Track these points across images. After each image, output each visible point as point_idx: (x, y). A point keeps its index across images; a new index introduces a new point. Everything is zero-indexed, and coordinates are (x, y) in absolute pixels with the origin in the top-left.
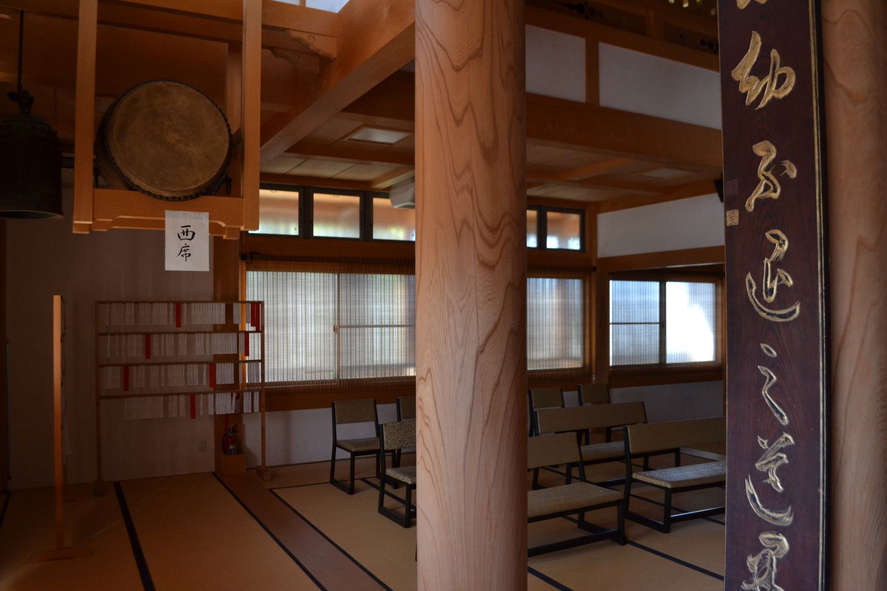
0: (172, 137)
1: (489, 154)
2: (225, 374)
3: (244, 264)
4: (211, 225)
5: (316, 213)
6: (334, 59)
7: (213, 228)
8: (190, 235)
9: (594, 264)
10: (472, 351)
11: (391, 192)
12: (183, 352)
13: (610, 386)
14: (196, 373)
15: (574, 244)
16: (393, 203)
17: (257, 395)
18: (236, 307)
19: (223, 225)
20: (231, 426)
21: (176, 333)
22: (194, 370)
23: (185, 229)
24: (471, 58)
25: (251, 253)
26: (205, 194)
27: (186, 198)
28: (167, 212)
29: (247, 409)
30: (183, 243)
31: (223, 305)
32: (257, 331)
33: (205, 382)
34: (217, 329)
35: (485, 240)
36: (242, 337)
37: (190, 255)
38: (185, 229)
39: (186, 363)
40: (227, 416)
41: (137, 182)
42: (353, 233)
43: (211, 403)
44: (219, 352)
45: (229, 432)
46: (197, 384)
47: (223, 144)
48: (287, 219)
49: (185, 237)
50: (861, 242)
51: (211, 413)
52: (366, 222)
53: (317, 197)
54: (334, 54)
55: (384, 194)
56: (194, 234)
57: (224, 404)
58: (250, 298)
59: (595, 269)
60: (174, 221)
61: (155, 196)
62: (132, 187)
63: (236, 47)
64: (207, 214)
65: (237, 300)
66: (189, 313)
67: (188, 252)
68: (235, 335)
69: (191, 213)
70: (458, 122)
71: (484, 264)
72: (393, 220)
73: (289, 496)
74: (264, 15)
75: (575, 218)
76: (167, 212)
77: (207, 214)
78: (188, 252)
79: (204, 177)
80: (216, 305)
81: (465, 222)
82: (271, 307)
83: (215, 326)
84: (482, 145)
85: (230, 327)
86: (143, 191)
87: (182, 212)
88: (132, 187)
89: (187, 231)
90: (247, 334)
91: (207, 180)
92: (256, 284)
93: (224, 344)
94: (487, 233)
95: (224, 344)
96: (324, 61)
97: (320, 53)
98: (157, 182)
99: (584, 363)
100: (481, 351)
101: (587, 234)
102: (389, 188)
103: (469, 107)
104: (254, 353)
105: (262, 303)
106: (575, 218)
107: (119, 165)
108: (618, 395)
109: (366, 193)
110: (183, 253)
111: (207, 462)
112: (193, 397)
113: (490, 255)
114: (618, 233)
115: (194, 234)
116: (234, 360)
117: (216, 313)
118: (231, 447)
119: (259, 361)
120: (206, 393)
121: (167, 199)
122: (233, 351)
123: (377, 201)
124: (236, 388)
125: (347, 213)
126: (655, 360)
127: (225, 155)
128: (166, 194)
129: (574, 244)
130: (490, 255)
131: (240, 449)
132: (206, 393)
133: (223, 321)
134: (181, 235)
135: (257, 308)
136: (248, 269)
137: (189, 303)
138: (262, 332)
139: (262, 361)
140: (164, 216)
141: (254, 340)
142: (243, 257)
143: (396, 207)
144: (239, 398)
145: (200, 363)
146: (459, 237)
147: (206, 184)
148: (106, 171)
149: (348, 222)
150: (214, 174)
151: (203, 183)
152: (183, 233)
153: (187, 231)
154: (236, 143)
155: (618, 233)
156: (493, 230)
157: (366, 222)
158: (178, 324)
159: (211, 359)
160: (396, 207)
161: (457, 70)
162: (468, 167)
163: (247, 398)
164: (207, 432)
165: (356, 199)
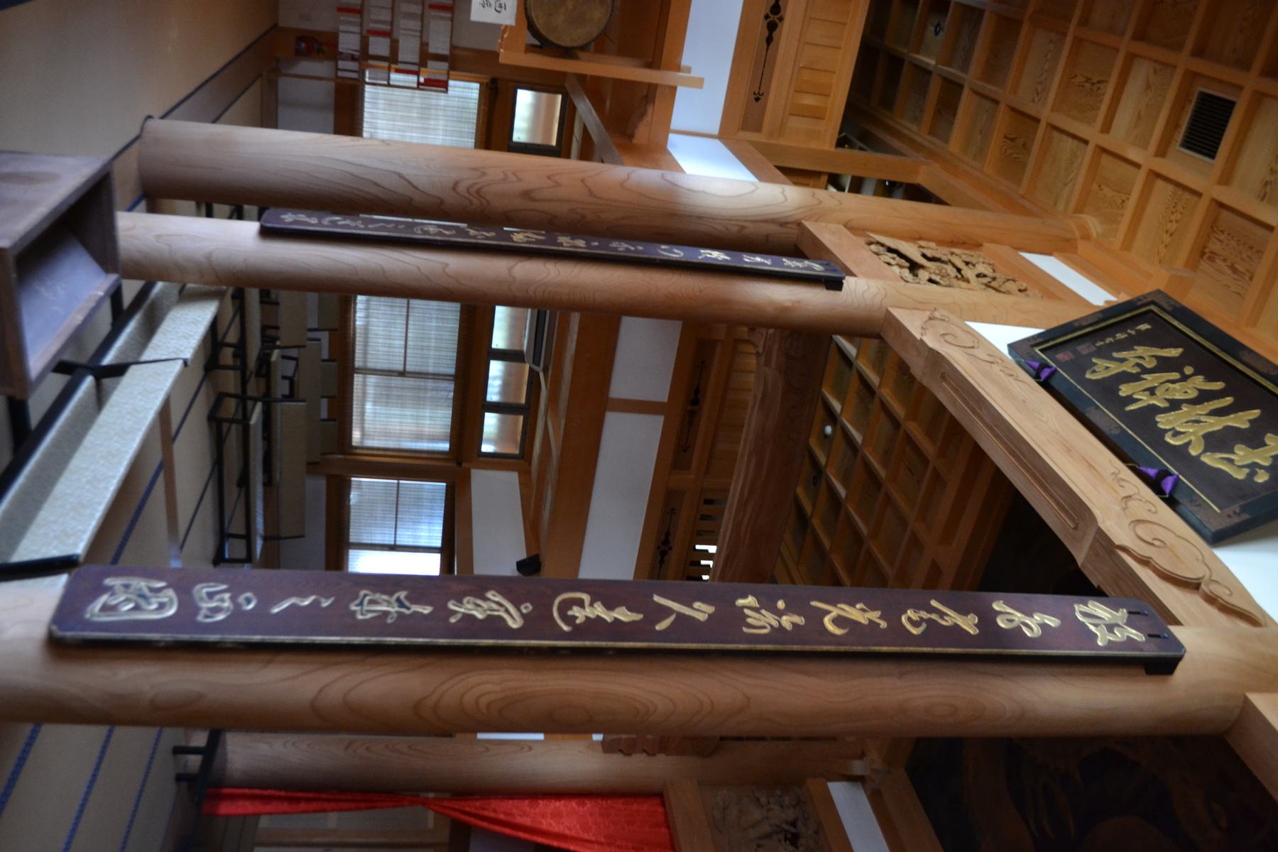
1: (527, 194)
2: (379, 46)
9: (464, 465)
10: (403, 171)
12: (404, 7)
13: (330, 478)
14: (382, 18)
15: (487, 448)
17: (355, 75)
18: (444, 66)
20: (325, 48)
21: (423, 4)
22: (385, 16)
24: (590, 191)
27: (526, 9)
29: (341, 64)
31: (447, 52)
32: (419, 83)
33: (373, 26)
34: (424, 45)
35: (471, 186)
36: (415, 68)
39: (393, 9)
40: (336, 46)
43: (351, 28)
44: (402, 44)
45: (319, 45)
46: (372, 17)
47: (566, 42)
50: (447, 265)
51: (342, 28)
54: (634, 141)
57: (349, 42)
58: (451, 83)
59: (459, 464)
63: (650, 65)
65: (452, 68)
66: (442, 18)
68: (416, 60)
69: (515, 11)
70: (549, 177)
71: (456, 184)
73: (255, 89)
75: (515, 451)
80: (447, 46)
81: (484, 174)
82: (442, 103)
83: (427, 44)
84: (533, 190)
85: (425, 57)
90: (417, 73)
92: (466, 93)
93: (408, 50)
94: (476, 187)
95: (408, 50)
96: (631, 136)
99: (356, 448)
100: (400, 176)
101: (496, 461)
103: (558, 185)
104: (396, 78)
105: (446, 92)
106: (515, 451)
108: (317, 487)
111: (290, 20)
112: (359, 11)
113: (462, 188)
114: (496, 496)
116: (392, 60)
117: (439, 45)
118: (303, 45)
119: (389, 80)
120: (361, 25)
122: (401, 57)
124: (364, 57)
126: (353, 539)
129: (487, 448)
130: (462, 188)
131: (300, 54)
132: (361, 25)
133: (432, 50)
135: (442, 85)
136: (481, 85)
137: (452, 20)
138: (418, 88)
139: (389, 85)
141: (411, 80)
142: (494, 81)
144: (353, 58)
145: (392, 23)
146: (475, 169)
155: (496, 496)
156: (478, 192)
158: (432, 7)
159: (395, 35)
161: (582, 181)
162: (520, 180)
163: (353, 65)
164: (320, 23)
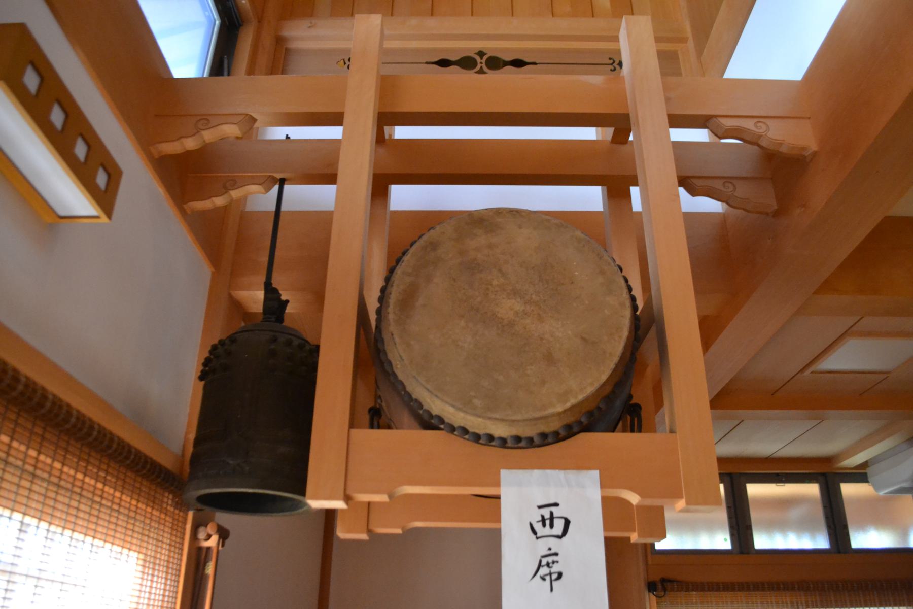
0: (508, 307)
3: (654, 598)
4: (605, 500)
5: (754, 515)
6: (815, 154)
7: (613, 509)
8: (559, 525)
11: (869, 471)
16: (877, 488)
19: (634, 499)
23: (546, 512)
25: (664, 580)
26: (588, 428)
27: (546, 439)
28: (504, 473)
30: (542, 547)
37: (560, 575)
38: (546, 512)
41: (436, 406)
42: (821, 542)
48: (710, 527)
49: (547, 531)
52: (836, 521)
53: (754, 490)
55: (859, 475)
56: (567, 523)
60: (522, 491)
61: (477, 438)
62: (429, 422)
64: (596, 474)
67: (556, 568)
72: (878, 516)
74: (668, 100)
76: (504, 473)
77: (596, 474)
78: (556, 568)
79: (586, 383)
86: (452, 429)
87: (537, 473)
88: (429, 422)
89: (552, 518)
91: (590, 390)
97: (784, 149)
98: (477, 402)
102: (865, 465)
107: (401, 376)
109: (828, 475)
110: (544, 571)
115: (567, 523)
121: (503, 443)
123: (848, 490)
125: (795, 513)
127: (625, 333)
128: (500, 431)
134: (538, 527)
140: (498, 484)
143: (881, 493)
147: (587, 399)
148: (383, 402)
149: (803, 526)
150: (604, 378)
151: (581, 397)
152: (543, 520)
153: (552, 518)
154: (645, 326)
157: (836, 521)
160: (881, 493)
165: (812, 490)
